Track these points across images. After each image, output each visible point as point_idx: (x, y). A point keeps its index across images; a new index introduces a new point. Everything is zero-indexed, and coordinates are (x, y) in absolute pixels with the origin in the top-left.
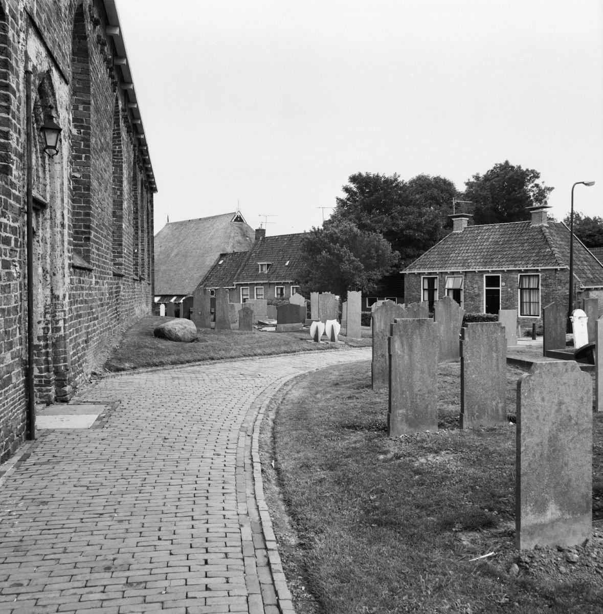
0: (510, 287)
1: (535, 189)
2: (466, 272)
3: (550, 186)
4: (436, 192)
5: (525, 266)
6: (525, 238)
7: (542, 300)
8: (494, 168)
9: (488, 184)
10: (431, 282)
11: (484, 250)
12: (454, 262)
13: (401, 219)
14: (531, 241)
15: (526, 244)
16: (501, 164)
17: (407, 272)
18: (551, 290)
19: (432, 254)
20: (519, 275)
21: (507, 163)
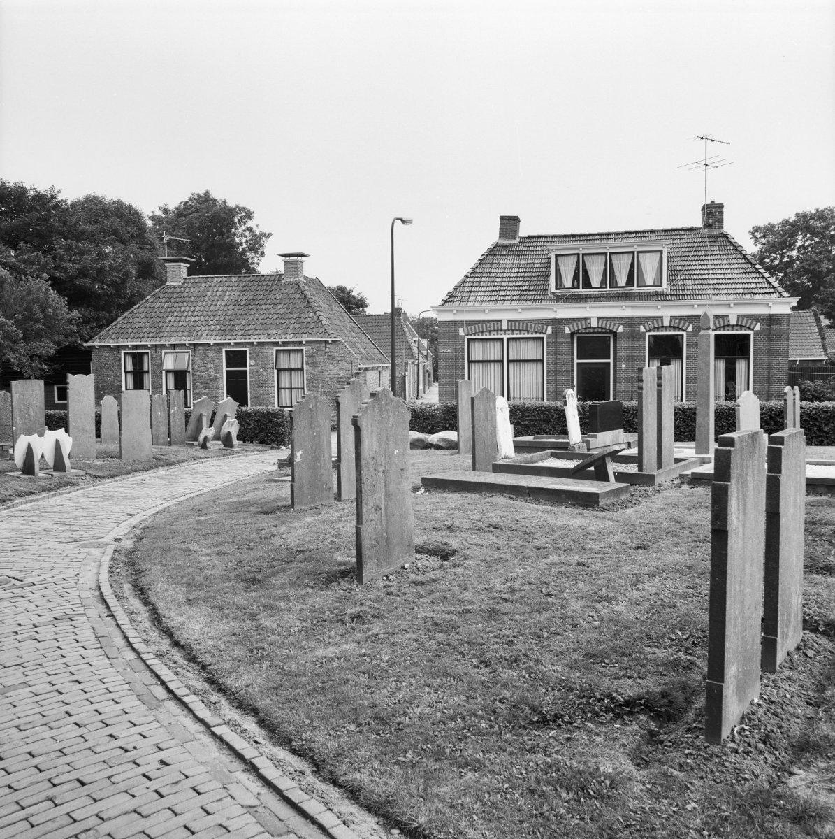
0: (263, 367)
1: (247, 233)
2: (195, 345)
3: (267, 232)
4: (117, 223)
5: (283, 336)
6: (278, 297)
7: (308, 385)
8: (190, 199)
9: (183, 220)
10: (138, 359)
11: (219, 313)
12: (173, 329)
13: (70, 260)
14: (287, 301)
15: (280, 306)
16: (199, 195)
17: (96, 344)
18: (320, 370)
19: (136, 318)
20: (275, 349)
21: (207, 193)
